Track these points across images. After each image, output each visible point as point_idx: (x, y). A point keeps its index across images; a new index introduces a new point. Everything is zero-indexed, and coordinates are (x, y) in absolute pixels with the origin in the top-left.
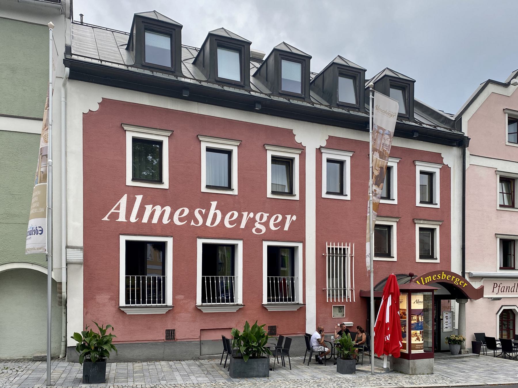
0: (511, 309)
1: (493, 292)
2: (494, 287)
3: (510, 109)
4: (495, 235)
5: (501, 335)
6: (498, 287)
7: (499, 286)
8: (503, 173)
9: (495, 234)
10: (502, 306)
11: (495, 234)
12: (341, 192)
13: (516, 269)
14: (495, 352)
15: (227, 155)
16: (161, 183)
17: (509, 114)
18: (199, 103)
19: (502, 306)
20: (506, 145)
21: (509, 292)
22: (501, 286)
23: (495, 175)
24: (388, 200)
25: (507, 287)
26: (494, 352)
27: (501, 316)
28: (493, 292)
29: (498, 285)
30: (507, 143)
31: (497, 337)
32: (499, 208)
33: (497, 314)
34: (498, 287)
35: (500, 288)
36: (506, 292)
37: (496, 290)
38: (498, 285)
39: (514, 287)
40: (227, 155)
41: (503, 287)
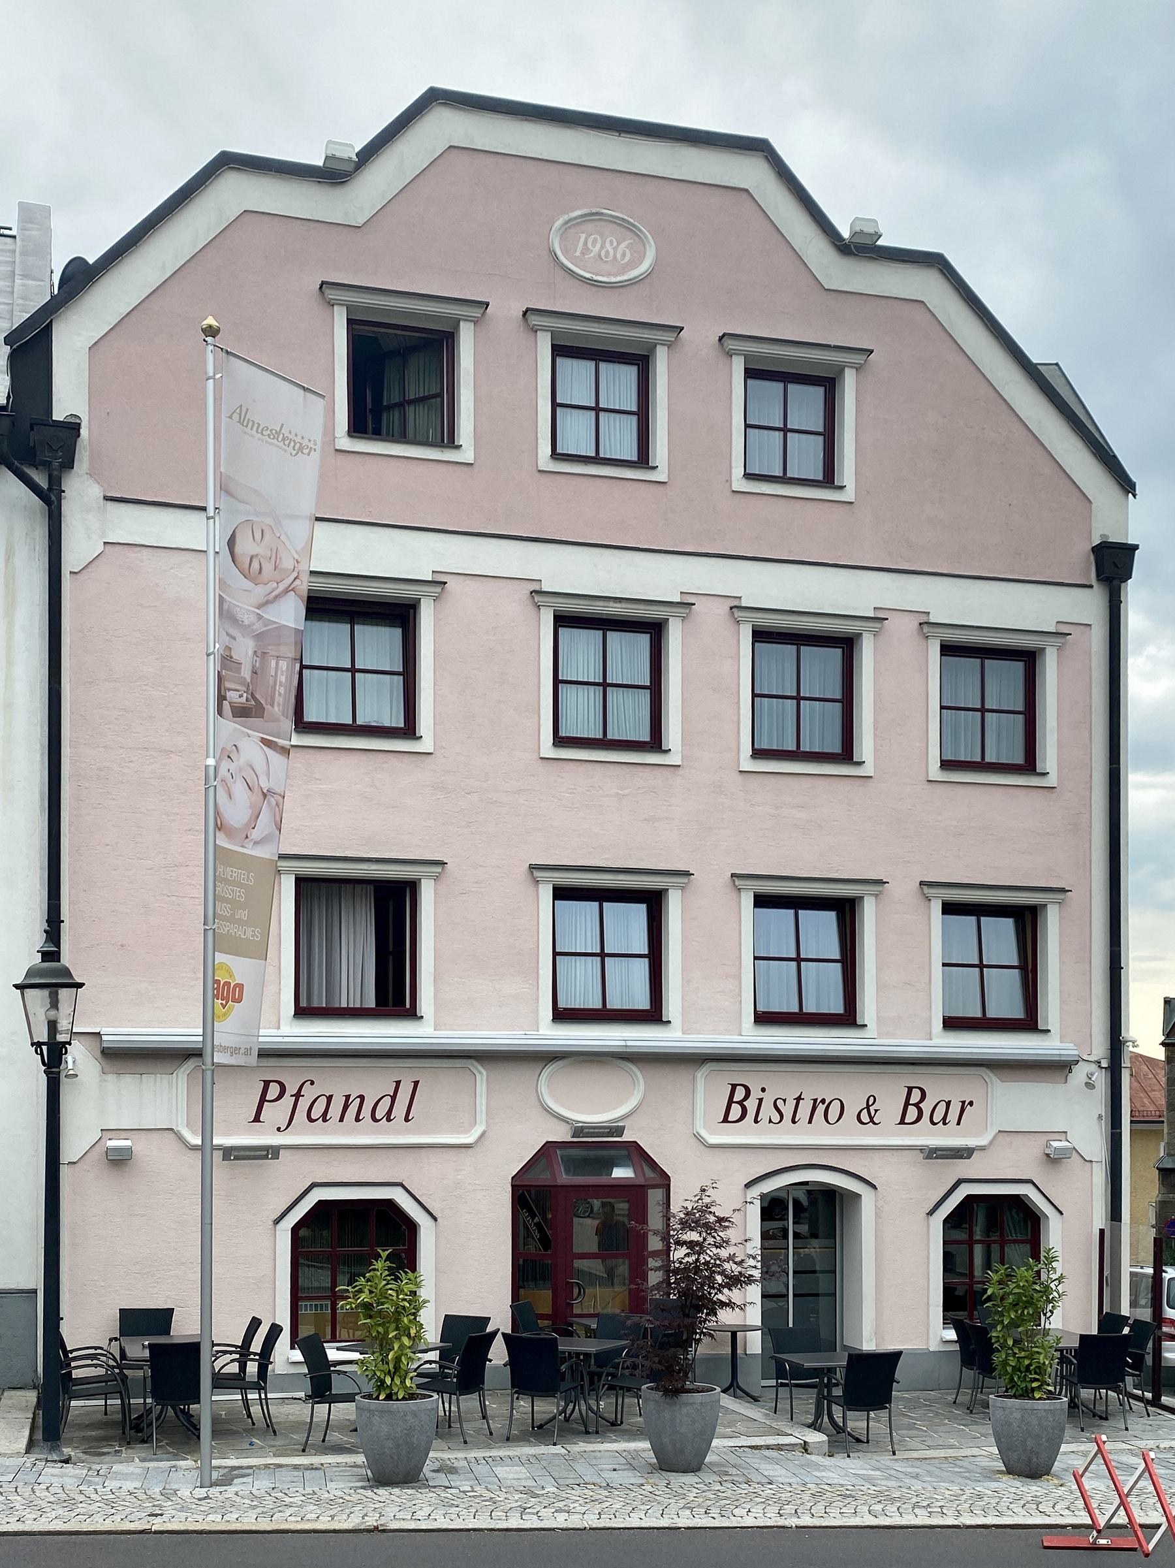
0: (1018, 1196)
1: (257, 1119)
2: (263, 1100)
3: (380, 290)
4: (922, 889)
5: (520, 1310)
6: (288, 1101)
7: (298, 1095)
8: (1011, 635)
9: (733, 875)
10: (314, 1185)
11: (733, 875)
12: (1026, 763)
13: (858, 1023)
14: (263, 1396)
15: (1020, 665)
16: (412, 736)
17: (349, 309)
18: (444, 450)
19: (314, 1185)
20: (540, 471)
21: (357, 1119)
22: (309, 1093)
23: (531, 610)
24: (848, 764)
25: (348, 1097)
26: (246, 1402)
27: (951, 1222)
28: (257, 1119)
29: (291, 1089)
30: (345, 443)
31: (501, 1320)
32: (747, 764)
33: (931, 1213)
34: (288, 1101)
35: (304, 1104)
36: (341, 1120)
37: (276, 1112)
38: (291, 1089)
39: (394, 1098)
40: (1020, 665)
41: (323, 1100)
